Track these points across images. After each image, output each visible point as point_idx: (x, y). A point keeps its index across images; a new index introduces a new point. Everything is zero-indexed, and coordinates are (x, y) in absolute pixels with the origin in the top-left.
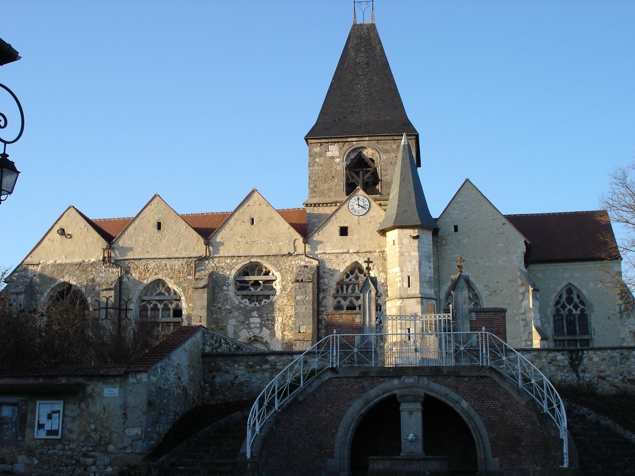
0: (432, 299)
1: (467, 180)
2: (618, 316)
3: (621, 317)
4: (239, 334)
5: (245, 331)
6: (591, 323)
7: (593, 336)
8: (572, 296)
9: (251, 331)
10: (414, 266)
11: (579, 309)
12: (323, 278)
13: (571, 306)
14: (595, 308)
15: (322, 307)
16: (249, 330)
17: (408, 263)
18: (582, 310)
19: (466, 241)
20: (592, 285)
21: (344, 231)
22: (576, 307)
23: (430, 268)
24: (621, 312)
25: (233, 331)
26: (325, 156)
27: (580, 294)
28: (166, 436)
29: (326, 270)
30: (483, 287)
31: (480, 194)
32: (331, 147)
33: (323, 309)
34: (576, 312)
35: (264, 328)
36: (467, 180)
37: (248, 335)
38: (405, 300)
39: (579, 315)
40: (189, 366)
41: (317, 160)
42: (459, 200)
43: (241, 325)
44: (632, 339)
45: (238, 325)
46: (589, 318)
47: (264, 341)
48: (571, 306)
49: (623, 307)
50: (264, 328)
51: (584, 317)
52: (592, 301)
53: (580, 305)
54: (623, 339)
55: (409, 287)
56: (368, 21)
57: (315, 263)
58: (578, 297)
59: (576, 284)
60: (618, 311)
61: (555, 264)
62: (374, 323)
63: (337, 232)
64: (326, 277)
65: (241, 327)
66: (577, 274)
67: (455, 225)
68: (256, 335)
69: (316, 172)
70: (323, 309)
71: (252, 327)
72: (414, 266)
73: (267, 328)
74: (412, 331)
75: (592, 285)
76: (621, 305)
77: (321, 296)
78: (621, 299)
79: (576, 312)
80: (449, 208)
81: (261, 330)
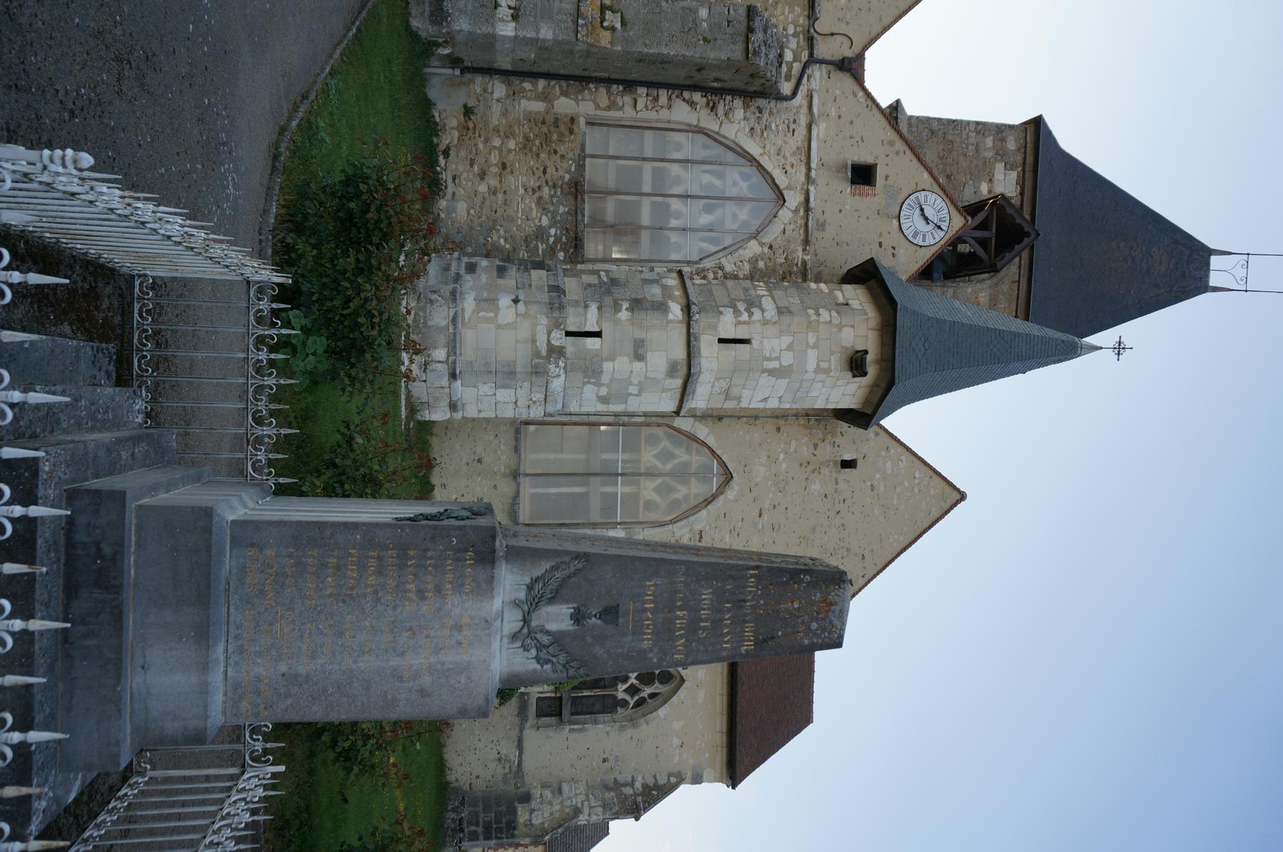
0: (681, 401)
1: (963, 497)
2: (609, 779)
3: (607, 787)
6: (596, 722)
7: (567, 728)
8: (657, 684)
10: (778, 358)
11: (627, 697)
12: (746, 106)
13: (635, 682)
14: (630, 732)
15: (670, 98)
17: (786, 340)
18: (624, 703)
19: (816, 487)
20: (677, 725)
21: (863, 175)
22: (632, 690)
23: (765, 400)
24: (617, 785)
26: (996, 160)
27: (660, 699)
29: (766, 115)
30: (698, 527)
31: (926, 525)
32: (1013, 175)
33: (663, 99)
34: (621, 691)
36: (963, 497)
38: (683, 328)
39: (615, 697)
41: (989, 142)
42: (917, 474)
44: (557, 815)
46: (608, 717)
48: (635, 682)
49: (628, 791)
51: (610, 705)
52: (644, 727)
53: (636, 698)
54: (560, 791)
55: (721, 341)
56: (1214, 280)
57: (786, 88)
58: (653, 696)
59: (682, 693)
60: (621, 778)
62: (551, 688)
63: (866, 158)
64: (748, 114)
66: (701, 695)
67: (859, 463)
69: (964, 136)
70: (663, 99)
72: (778, 358)
74: (591, 343)
75: (677, 725)
76: (632, 784)
77: (697, 97)
78: (645, 786)
79: (621, 691)
80: (900, 449)
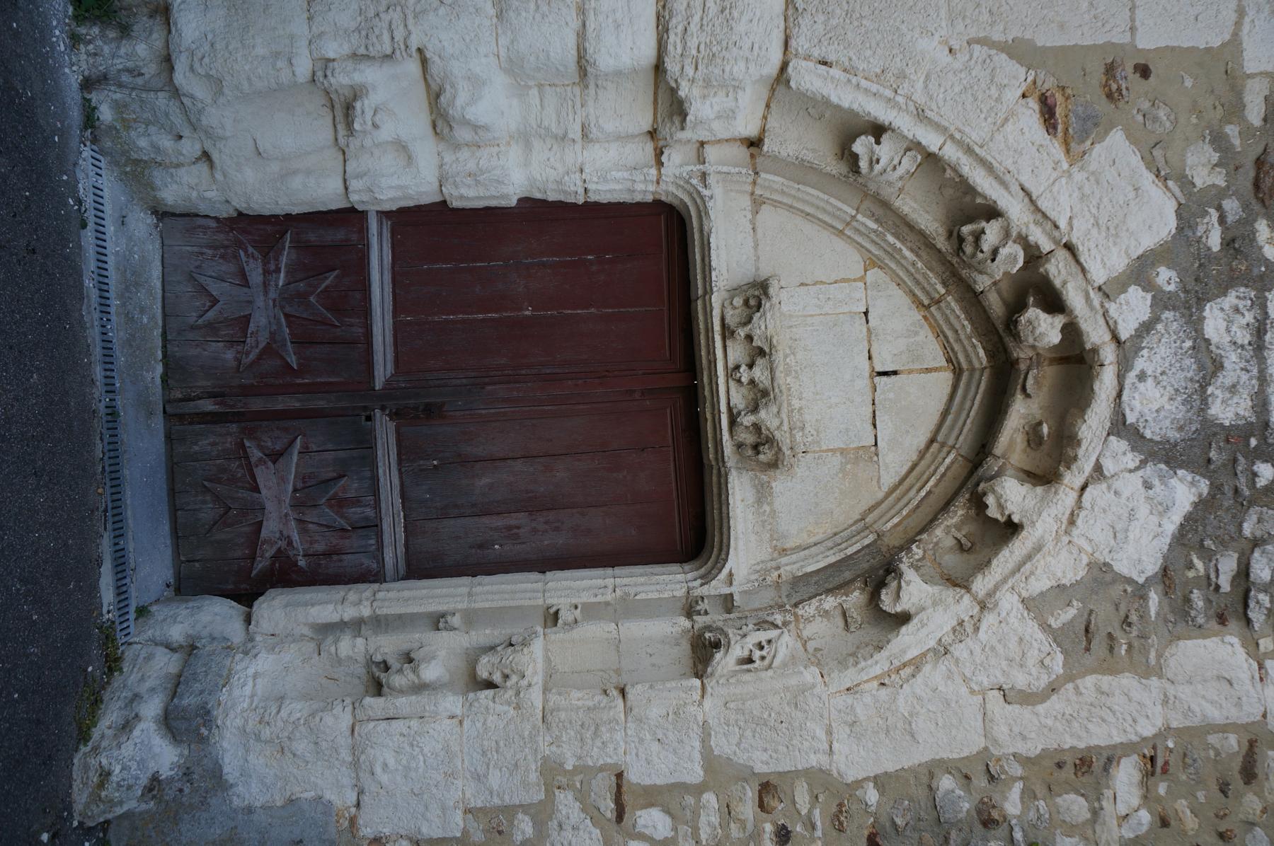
4: (1117, 137)
5: (1155, 218)
6: (187, 601)
9: (1161, 302)
16: (1166, 278)
25: (1145, 42)
28: (596, 206)
35: (1184, 492)
37: (1105, 261)
40: (1102, 365)
43: (1227, 158)
45: (1235, 110)
47: (1012, 495)
50: (1184, 492)
61: (466, 580)
65: (1203, 169)
68: (1105, 383)
71: (1215, 322)
73: (1191, 535)
81: (1166, 455)
